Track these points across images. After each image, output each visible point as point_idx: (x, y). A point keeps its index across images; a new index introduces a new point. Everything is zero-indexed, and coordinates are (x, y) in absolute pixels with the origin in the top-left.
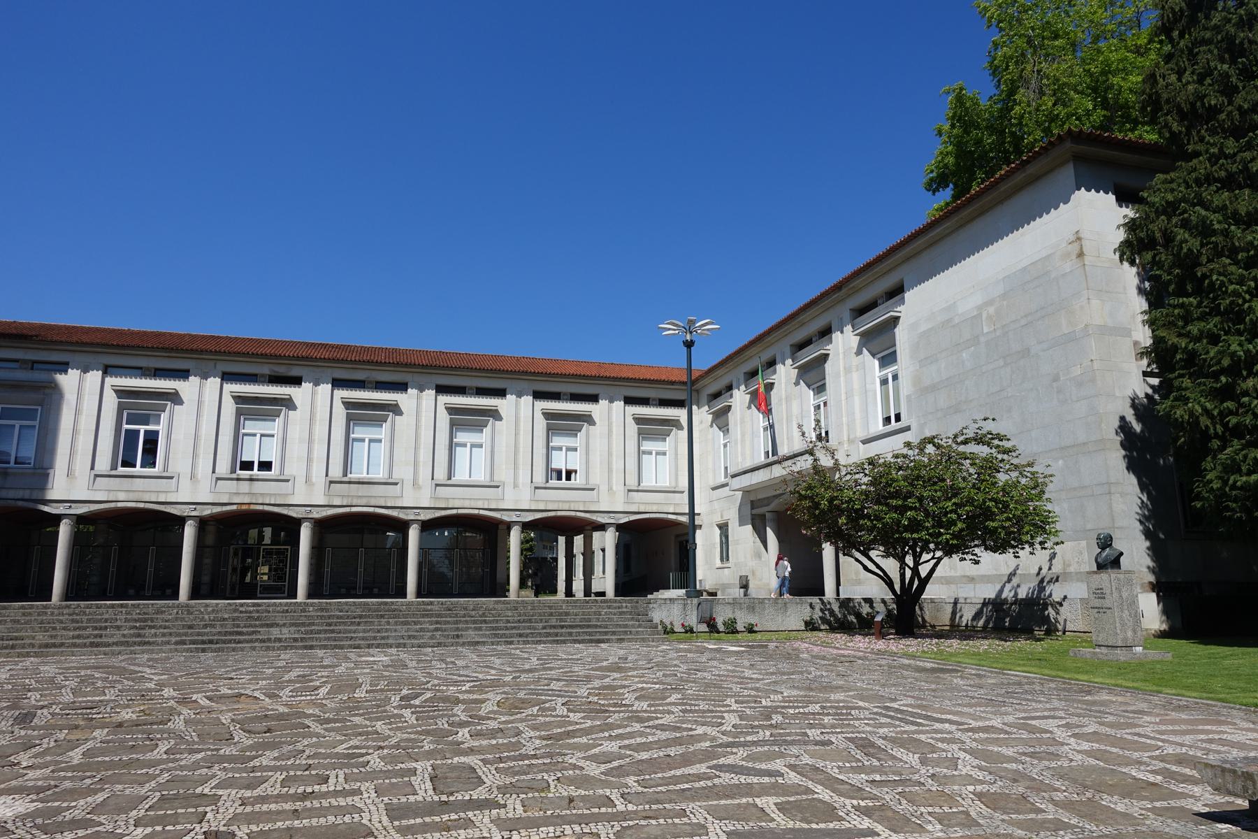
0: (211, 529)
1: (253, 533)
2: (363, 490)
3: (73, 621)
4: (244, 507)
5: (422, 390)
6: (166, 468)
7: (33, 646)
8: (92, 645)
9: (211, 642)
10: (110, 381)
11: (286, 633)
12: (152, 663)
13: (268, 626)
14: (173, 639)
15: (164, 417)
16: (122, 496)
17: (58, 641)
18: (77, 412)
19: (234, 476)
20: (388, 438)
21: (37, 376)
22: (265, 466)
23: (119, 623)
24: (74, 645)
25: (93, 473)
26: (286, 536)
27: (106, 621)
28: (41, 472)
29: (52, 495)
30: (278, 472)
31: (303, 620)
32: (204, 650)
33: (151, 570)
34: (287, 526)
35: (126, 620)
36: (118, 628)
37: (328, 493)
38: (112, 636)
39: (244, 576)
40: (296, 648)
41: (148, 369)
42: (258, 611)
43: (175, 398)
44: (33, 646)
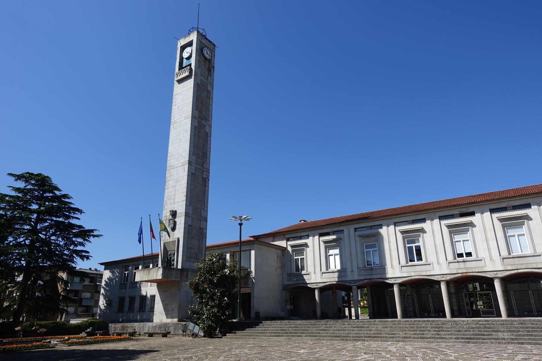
0: (452, 285)
1: (470, 286)
2: (522, 261)
3: (411, 327)
4: (464, 274)
5: (388, 226)
6: (307, 271)
7: (399, 337)
8: (421, 338)
9: (470, 339)
10: (398, 228)
11: (506, 335)
12: (449, 347)
13: (496, 331)
14: (454, 337)
15: (421, 239)
16: (413, 274)
17: (408, 336)
18: (389, 243)
19: (456, 261)
20: (528, 233)
21: (373, 231)
22: (469, 254)
23: (428, 329)
24: (415, 338)
25: (400, 265)
26: (486, 286)
27: (423, 328)
28: (382, 267)
29: (389, 276)
30: (475, 257)
31: (513, 329)
32: (468, 342)
33: (431, 305)
34: (487, 282)
35: (431, 328)
36: (429, 331)
37: (503, 264)
38: (428, 334)
39: (472, 307)
40: (514, 343)
41: (410, 221)
42: (488, 324)
43: (422, 231)
44: (399, 337)
